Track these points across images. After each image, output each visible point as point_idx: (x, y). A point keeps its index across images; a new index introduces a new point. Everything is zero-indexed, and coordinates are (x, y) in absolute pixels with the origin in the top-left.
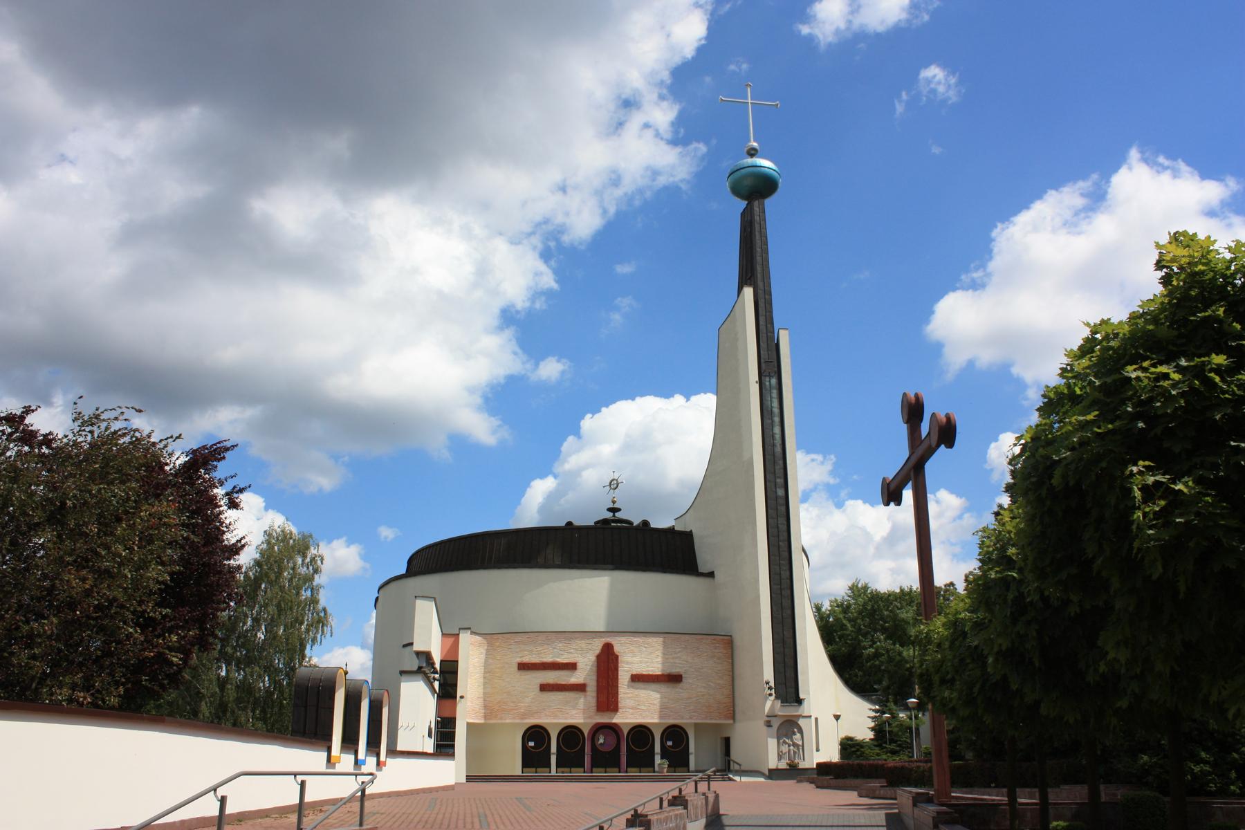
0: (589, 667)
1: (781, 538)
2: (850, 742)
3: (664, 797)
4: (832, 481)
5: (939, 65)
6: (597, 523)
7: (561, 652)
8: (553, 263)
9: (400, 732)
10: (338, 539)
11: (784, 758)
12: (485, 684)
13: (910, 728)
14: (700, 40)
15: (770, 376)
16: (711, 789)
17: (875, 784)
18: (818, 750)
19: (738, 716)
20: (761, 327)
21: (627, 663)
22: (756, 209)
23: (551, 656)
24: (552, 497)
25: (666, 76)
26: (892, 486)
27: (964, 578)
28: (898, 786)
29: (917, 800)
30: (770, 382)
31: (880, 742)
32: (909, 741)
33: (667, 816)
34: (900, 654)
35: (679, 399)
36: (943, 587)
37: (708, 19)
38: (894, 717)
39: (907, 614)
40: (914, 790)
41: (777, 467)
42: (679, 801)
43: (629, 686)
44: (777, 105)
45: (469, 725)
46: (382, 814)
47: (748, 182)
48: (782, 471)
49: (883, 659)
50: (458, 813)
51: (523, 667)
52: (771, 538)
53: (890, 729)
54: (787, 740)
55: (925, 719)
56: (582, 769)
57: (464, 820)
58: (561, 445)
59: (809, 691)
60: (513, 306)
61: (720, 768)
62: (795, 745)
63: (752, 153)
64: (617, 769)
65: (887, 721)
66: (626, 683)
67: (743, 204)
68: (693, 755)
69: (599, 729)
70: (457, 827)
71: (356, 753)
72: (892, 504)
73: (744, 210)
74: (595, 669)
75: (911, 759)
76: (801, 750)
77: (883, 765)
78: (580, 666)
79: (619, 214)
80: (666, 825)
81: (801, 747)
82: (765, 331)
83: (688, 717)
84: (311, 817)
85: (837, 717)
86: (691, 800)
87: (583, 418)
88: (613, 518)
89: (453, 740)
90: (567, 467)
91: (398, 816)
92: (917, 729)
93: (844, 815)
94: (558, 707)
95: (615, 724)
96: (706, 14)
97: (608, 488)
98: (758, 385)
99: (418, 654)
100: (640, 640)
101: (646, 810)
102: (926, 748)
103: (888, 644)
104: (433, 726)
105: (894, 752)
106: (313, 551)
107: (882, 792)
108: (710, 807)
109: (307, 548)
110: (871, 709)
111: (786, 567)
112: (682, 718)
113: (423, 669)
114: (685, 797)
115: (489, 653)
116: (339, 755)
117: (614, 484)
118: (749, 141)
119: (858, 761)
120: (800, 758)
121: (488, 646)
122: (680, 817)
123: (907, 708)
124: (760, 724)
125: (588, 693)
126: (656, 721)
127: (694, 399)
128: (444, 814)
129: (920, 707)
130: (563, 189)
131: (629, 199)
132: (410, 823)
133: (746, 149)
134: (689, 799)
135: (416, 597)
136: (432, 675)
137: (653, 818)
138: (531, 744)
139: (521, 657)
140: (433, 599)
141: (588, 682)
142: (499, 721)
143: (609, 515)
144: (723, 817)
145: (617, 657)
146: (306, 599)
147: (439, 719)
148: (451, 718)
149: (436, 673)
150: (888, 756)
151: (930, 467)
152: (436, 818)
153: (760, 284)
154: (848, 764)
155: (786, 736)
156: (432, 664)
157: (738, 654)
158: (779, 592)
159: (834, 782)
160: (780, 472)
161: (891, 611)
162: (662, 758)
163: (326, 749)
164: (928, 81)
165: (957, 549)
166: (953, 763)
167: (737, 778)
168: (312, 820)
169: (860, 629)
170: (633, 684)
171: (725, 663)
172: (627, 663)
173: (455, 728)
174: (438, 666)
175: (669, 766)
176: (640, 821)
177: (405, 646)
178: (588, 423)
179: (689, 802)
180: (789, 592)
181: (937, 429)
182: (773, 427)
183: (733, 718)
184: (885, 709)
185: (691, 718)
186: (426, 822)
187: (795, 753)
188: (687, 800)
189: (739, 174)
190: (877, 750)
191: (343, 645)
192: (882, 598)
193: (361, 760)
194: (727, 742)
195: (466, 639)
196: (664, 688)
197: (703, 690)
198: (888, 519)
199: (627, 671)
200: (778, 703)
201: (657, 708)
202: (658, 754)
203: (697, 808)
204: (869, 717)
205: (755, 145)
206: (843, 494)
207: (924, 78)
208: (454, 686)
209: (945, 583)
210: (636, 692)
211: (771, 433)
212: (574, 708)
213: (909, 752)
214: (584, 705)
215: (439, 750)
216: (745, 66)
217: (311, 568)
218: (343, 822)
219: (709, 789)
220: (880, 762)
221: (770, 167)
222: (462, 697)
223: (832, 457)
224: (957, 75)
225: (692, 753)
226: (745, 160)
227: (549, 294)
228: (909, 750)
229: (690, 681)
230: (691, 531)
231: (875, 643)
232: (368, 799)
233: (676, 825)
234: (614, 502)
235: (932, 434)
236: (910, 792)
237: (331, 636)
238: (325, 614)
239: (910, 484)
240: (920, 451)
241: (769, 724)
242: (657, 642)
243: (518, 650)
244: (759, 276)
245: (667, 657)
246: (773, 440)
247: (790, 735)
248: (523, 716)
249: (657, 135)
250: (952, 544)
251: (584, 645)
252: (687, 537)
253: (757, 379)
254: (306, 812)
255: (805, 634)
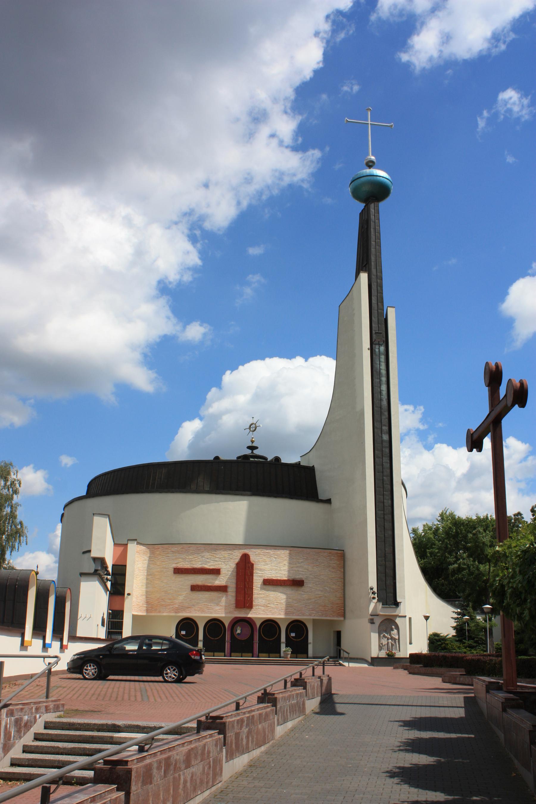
0: (230, 573)
1: (385, 474)
2: (436, 638)
3: (288, 680)
4: (421, 427)
5: (514, 89)
6: (238, 458)
7: (208, 560)
8: (199, 245)
9: (80, 622)
10: (27, 466)
11: (384, 649)
12: (147, 584)
13: (485, 629)
14: (318, 63)
15: (380, 345)
16: (325, 673)
17: (457, 672)
18: (411, 643)
19: (348, 614)
20: (373, 305)
21: (261, 570)
22: (372, 210)
23: (200, 563)
24: (199, 436)
25: (290, 93)
26: (475, 437)
27: (531, 508)
28: (474, 675)
29: (490, 687)
30: (379, 349)
31: (460, 638)
32: (484, 638)
33: (290, 695)
34: (478, 569)
35: (299, 360)
36: (513, 516)
37: (324, 47)
38: (472, 619)
39: (486, 538)
40: (487, 679)
41: (383, 417)
42: (299, 682)
43: (262, 589)
44: (392, 126)
45: (134, 616)
46: (64, 687)
47: (366, 188)
48: (387, 420)
49: (464, 572)
50: (125, 687)
51: (178, 571)
52: (377, 473)
53: (469, 628)
54: (386, 635)
55: (497, 620)
56: (223, 654)
57: (129, 693)
58: (207, 394)
59: (405, 596)
60: (166, 278)
61: (332, 655)
62: (392, 638)
63: (370, 164)
64: (251, 654)
65: (467, 621)
66: (259, 586)
67: (362, 205)
68: (312, 644)
69: (237, 621)
70: (123, 699)
71: (44, 638)
72: (475, 450)
73: (362, 211)
74: (235, 574)
75: (485, 653)
76: (397, 643)
77: (463, 657)
78: (223, 571)
79: (250, 206)
80: (289, 702)
81: (397, 641)
82: (376, 308)
83: (307, 614)
84: (7, 690)
85: (427, 618)
86: (309, 682)
87: (224, 374)
88: (252, 454)
89: (122, 629)
90: (211, 410)
91: (76, 689)
92: (491, 630)
93: (430, 697)
94: (206, 604)
95: (250, 618)
96: (323, 42)
97: (248, 430)
98: (369, 351)
99: (95, 559)
100: (271, 552)
101: (274, 689)
102: (497, 644)
103: (470, 561)
104: (105, 617)
105: (471, 647)
106: (13, 476)
107: (461, 679)
108: (324, 688)
109: (9, 473)
110: (454, 612)
111: (388, 497)
112: (303, 615)
113: (98, 572)
114: (304, 679)
115: (151, 560)
116: (30, 640)
117: (253, 428)
118: (368, 155)
119: (443, 654)
120: (396, 649)
121: (150, 554)
122: (301, 696)
123: (483, 612)
124: (365, 622)
125: (229, 593)
126: (282, 616)
127: (311, 359)
128: (113, 688)
129: (493, 611)
130: (206, 186)
131: (260, 193)
132: (86, 695)
133: (365, 162)
134: (307, 681)
135: (94, 514)
136: (106, 576)
137: (279, 696)
138: (293, 635)
139: (176, 563)
140: (107, 516)
141: (229, 584)
142: (158, 614)
143: (249, 452)
144: (334, 696)
145: (253, 565)
146: (6, 514)
147: (110, 611)
148: (120, 611)
149: (109, 574)
150: (467, 650)
151: (505, 422)
152: (107, 691)
153: (374, 271)
154: (434, 655)
155: (386, 631)
156: (106, 568)
157: (348, 563)
158: (383, 516)
159: (423, 670)
160: (385, 421)
161: (474, 534)
162: (287, 646)
163: (20, 635)
164: (506, 102)
165: (523, 485)
166: (519, 657)
167: (346, 664)
168: (8, 691)
169: (446, 548)
170: (265, 587)
171: (338, 571)
172: (261, 570)
173: (123, 619)
174: (110, 569)
175: (292, 653)
176: (269, 698)
177: (84, 553)
178: (228, 377)
179: (307, 684)
180: (390, 516)
181: (512, 392)
182: (380, 385)
183: (344, 615)
184: (465, 612)
185: (310, 615)
186: (99, 695)
187: (392, 645)
188: (306, 682)
189: (359, 181)
190: (458, 644)
191: (33, 551)
192: (463, 523)
193: (48, 644)
194: (338, 634)
195: (132, 548)
196: (289, 590)
197: (320, 593)
198: (467, 460)
199: (260, 576)
200: (380, 605)
201: (283, 606)
202: (283, 643)
203: (313, 688)
204: (452, 618)
205: (373, 158)
206: (431, 438)
207: (502, 100)
208: (123, 585)
209: (514, 513)
210: (268, 593)
211: (379, 390)
212: (218, 605)
213: (484, 647)
214: (226, 602)
215: (109, 636)
216: (356, 88)
217: (11, 490)
218: (32, 694)
219: (324, 673)
220: (460, 655)
221: (384, 176)
222: (129, 594)
223: (422, 407)
224: (529, 97)
225: (310, 643)
226: (364, 171)
227: (194, 269)
228: (483, 646)
229: (310, 586)
230: (313, 466)
231: (458, 559)
232: (54, 675)
233: (297, 702)
234: (252, 442)
235: (508, 395)
236: (484, 681)
237: (26, 544)
238: (22, 527)
239: (490, 434)
240: (498, 409)
241: (372, 622)
242: (284, 554)
243: (174, 558)
244: (373, 264)
245: (292, 566)
246: (381, 395)
247: (389, 630)
248: (177, 610)
249: (281, 143)
250: (519, 481)
251: (226, 555)
252: (310, 471)
253: (369, 347)
254: (4, 685)
255: (402, 551)
